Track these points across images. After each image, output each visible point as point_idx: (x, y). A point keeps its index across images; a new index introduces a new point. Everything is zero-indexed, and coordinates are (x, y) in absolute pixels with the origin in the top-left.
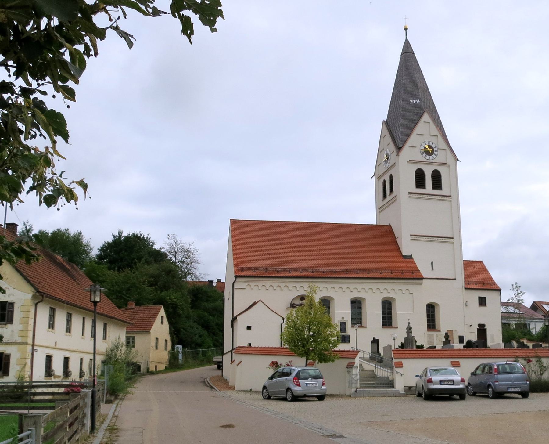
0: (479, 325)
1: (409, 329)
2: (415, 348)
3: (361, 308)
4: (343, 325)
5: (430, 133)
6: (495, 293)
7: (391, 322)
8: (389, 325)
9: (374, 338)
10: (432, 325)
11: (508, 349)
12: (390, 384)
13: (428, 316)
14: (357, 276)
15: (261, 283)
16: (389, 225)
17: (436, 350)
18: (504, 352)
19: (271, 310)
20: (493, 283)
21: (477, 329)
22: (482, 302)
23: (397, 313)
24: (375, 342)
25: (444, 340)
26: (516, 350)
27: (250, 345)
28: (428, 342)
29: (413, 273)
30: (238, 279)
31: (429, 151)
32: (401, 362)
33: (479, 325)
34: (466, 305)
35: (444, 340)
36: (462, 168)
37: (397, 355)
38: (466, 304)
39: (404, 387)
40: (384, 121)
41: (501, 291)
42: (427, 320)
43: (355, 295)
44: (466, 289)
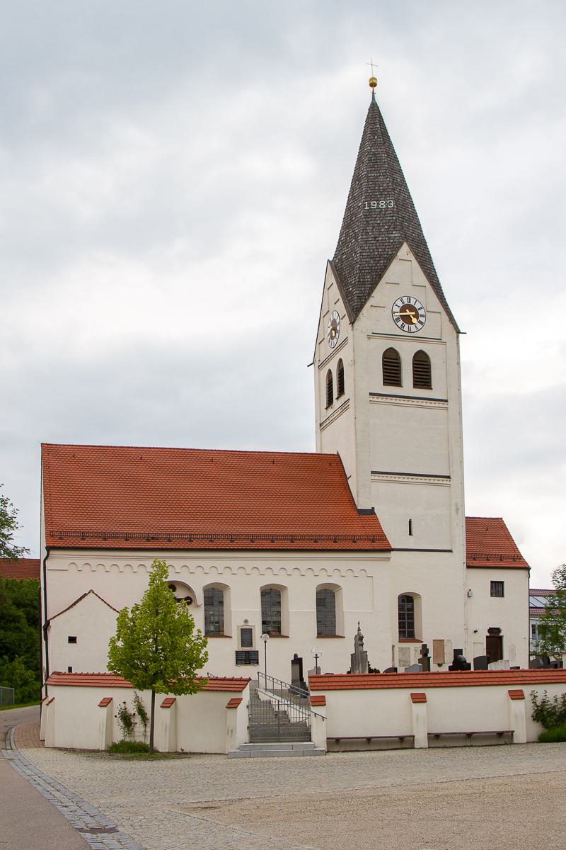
0: (490, 630)
1: (360, 638)
2: (367, 673)
3: (279, 603)
4: (246, 635)
5: (412, 282)
6: (521, 574)
7: (413, 632)
8: (409, 636)
9: (296, 655)
10: (409, 632)
11: (481, 671)
12: (306, 734)
13: (401, 616)
14: (336, 546)
15: (94, 559)
16: (336, 453)
17: (396, 675)
18: (448, 676)
19: (111, 607)
20: (518, 557)
21: (487, 637)
22: (497, 589)
23: (231, 611)
24: (297, 662)
25: (421, 656)
26: (472, 673)
27: (70, 669)
28: (400, 660)
29: (373, 541)
30: (51, 552)
31: (409, 316)
32: (424, 694)
33: (490, 630)
34: (469, 597)
35: (421, 656)
36: (470, 349)
37: (316, 684)
38: (468, 594)
39: (328, 739)
40: (328, 260)
41: (531, 571)
42: (400, 623)
43: (269, 580)
44: (468, 567)
